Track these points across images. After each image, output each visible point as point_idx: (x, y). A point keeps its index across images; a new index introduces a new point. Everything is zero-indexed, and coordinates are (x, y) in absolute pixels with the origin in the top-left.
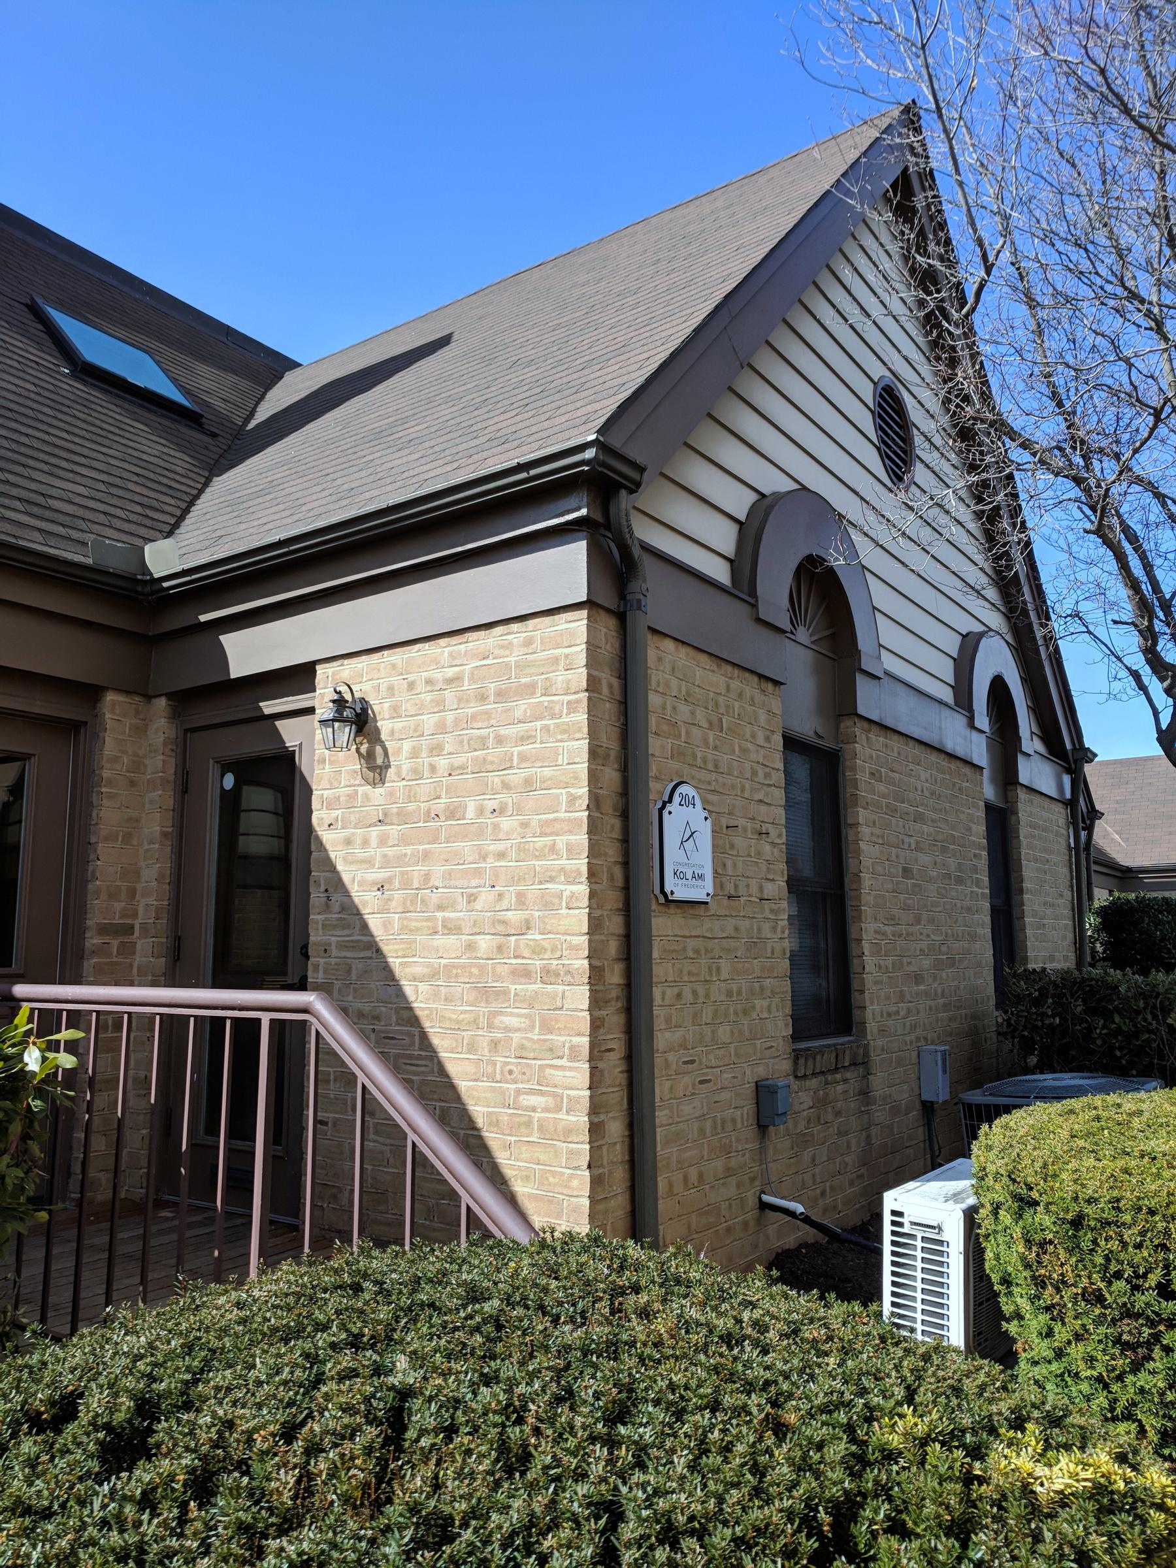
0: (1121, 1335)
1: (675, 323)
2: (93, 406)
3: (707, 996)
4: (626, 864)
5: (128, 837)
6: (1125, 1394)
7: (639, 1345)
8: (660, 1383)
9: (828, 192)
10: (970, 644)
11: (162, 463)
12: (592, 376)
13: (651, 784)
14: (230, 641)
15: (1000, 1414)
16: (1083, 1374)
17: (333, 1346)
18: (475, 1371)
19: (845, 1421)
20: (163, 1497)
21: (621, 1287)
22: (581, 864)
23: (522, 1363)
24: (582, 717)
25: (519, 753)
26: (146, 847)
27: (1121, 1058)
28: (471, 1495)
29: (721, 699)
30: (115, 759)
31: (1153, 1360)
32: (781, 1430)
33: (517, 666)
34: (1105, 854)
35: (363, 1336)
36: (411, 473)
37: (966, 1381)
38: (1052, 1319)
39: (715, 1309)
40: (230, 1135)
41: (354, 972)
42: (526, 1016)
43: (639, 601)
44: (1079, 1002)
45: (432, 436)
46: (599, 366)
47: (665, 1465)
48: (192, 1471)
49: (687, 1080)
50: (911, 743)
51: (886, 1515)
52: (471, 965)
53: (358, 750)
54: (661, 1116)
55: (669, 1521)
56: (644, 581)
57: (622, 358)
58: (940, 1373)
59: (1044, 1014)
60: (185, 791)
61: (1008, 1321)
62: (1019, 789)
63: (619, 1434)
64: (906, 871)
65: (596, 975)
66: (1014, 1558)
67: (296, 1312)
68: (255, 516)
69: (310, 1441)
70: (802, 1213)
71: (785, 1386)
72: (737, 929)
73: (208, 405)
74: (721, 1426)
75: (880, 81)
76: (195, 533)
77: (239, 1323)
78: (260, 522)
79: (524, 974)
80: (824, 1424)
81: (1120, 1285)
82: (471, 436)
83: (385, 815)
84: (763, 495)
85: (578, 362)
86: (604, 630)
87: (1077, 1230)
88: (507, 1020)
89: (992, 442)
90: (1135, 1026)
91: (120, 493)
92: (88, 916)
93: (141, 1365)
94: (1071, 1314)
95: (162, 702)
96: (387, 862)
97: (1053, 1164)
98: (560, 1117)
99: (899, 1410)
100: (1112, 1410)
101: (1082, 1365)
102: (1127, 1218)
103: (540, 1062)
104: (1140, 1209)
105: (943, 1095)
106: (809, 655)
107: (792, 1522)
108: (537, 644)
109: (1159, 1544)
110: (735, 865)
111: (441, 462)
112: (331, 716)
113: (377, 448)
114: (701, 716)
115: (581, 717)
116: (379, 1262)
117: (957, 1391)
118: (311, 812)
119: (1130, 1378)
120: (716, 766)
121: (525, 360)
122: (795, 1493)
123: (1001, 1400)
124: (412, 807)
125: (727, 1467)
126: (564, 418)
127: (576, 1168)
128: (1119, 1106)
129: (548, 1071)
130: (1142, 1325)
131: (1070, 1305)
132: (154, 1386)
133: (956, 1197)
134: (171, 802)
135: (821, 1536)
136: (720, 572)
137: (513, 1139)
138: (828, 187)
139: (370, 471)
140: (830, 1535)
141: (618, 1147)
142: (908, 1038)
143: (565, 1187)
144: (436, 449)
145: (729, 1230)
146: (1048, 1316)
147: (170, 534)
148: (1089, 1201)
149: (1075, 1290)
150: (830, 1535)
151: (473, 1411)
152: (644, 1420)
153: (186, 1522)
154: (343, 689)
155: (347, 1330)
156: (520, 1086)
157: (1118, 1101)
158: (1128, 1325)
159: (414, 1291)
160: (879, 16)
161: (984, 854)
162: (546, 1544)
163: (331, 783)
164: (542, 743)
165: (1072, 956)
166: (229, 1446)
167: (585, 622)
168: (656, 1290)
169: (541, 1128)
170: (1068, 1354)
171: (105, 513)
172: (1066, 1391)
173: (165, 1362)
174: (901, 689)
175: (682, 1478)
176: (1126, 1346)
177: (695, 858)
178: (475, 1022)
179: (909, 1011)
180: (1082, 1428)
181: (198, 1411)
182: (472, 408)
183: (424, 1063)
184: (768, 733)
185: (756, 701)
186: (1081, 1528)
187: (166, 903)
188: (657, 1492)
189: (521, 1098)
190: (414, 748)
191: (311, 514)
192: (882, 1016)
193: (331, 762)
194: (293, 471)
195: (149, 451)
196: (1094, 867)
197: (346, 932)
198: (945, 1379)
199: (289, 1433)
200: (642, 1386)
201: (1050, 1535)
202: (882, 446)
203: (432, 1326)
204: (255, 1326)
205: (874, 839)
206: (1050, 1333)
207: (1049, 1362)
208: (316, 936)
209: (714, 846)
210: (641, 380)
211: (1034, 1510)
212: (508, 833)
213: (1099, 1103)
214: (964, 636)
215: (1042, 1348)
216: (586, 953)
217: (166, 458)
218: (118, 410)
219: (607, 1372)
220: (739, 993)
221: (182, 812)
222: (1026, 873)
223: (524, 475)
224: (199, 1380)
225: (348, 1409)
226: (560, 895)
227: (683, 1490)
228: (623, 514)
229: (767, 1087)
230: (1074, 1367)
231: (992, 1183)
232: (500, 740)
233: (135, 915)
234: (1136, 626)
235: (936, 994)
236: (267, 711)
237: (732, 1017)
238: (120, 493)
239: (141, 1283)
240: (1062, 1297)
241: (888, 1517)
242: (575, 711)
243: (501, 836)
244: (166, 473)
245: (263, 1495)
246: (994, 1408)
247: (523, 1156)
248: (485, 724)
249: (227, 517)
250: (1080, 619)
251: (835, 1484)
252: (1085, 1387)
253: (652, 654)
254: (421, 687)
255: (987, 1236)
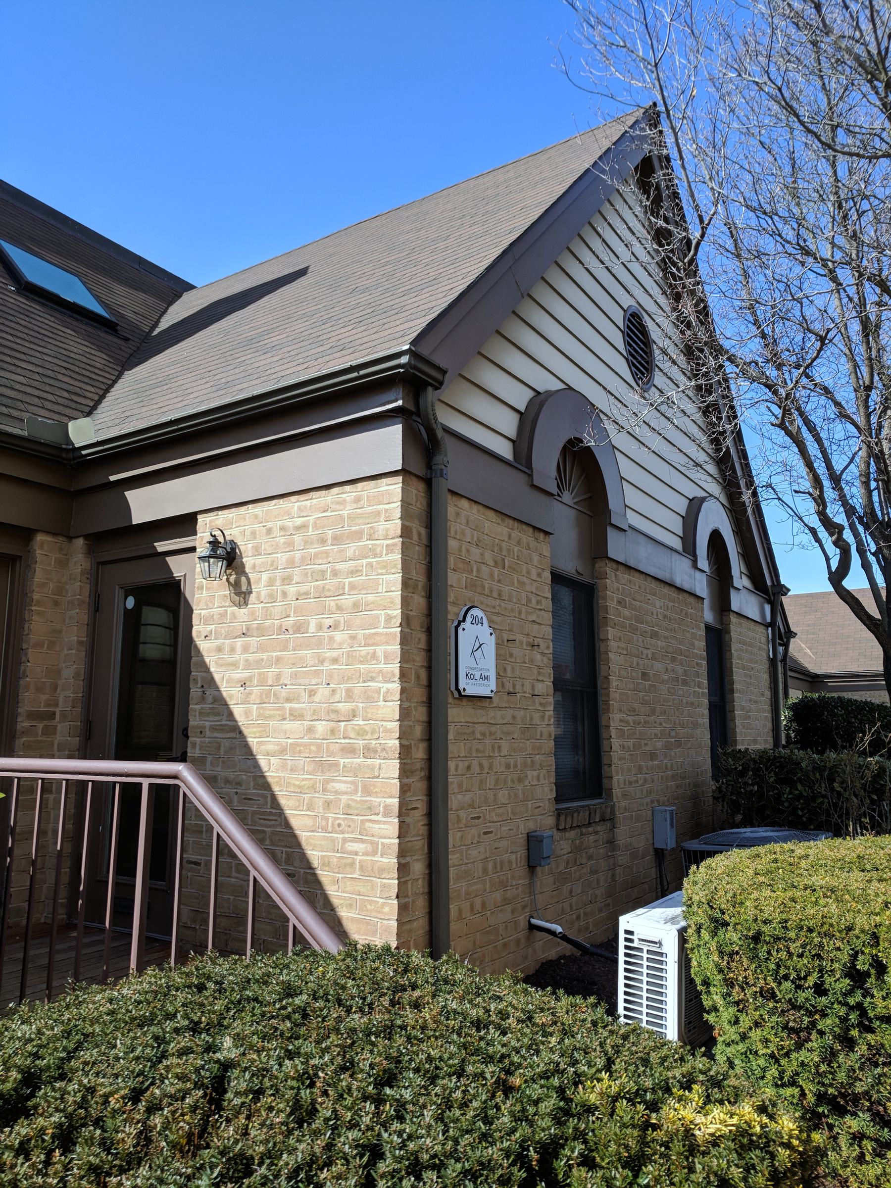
0: (788, 1022)
1: (472, 263)
2: (33, 316)
3: (490, 768)
4: (429, 668)
5: (52, 644)
6: (790, 1066)
7: (409, 1028)
8: (420, 1056)
9: (588, 170)
10: (695, 505)
11: (85, 360)
12: (410, 301)
13: (449, 607)
14: (132, 496)
15: (674, 1078)
16: (761, 1052)
17: (177, 1031)
18: (282, 1048)
19: (557, 1085)
20: (35, 1147)
21: (402, 986)
22: (395, 667)
23: (318, 1042)
24: (397, 557)
25: (350, 583)
26: (66, 652)
27: (802, 816)
28: (268, 1141)
29: (504, 545)
30: (43, 585)
31: (811, 1041)
32: (508, 1090)
33: (349, 518)
34: (799, 664)
35: (201, 1023)
36: (273, 371)
37: (653, 1054)
38: (738, 1011)
39: (470, 1002)
40: (117, 872)
41: (222, 748)
42: (352, 783)
43: (442, 470)
44: (772, 774)
45: (290, 343)
46: (415, 294)
47: (418, 1117)
48: (59, 1126)
49: (474, 831)
50: (649, 579)
51: (580, 1154)
52: (311, 744)
53: (228, 580)
54: (453, 859)
55: (417, 1158)
56: (446, 455)
57: (432, 288)
58: (634, 1048)
59: (746, 783)
60: (97, 610)
61: (708, 1013)
62: (731, 614)
63: (385, 1094)
64: (645, 676)
65: (405, 752)
66: (672, 1184)
67: (152, 1005)
68: (154, 401)
69: (151, 1102)
70: (560, 933)
71: (516, 1059)
72: (514, 717)
73: (122, 316)
74: (464, 1088)
75: (624, 89)
76: (109, 413)
77: (108, 1014)
78: (158, 406)
79: (350, 751)
80: (542, 1087)
81: (787, 985)
82: (318, 344)
83: (248, 629)
84: (538, 393)
85: (400, 290)
86: (415, 492)
87: (756, 943)
88: (337, 786)
89: (705, 357)
90: (812, 792)
91: (52, 382)
92: (20, 705)
93: (29, 1047)
94: (752, 1007)
95: (80, 542)
96: (248, 665)
97: (740, 895)
98: (376, 859)
99: (599, 1075)
100: (781, 1078)
101: (760, 1046)
102: (792, 935)
103: (362, 818)
104: (802, 928)
105: (671, 844)
106: (572, 513)
107: (508, 1157)
108: (364, 501)
109: (785, 1174)
110: (513, 669)
111: (295, 363)
112: (207, 554)
113: (248, 352)
114: (488, 557)
115: (396, 557)
116: (221, 967)
117: (646, 1062)
118: (192, 626)
119: (794, 1055)
120: (500, 595)
121: (362, 288)
122: (513, 1138)
123: (676, 1067)
124: (268, 623)
125: (463, 1118)
126: (387, 332)
127: (387, 898)
128: (793, 851)
129: (367, 824)
130: (803, 1015)
131: (751, 1000)
132: (38, 1062)
133: (673, 920)
134: (86, 617)
135: (530, 1169)
136: (504, 450)
137: (341, 876)
138: (588, 166)
139: (242, 369)
140: (537, 1168)
141: (420, 882)
142: (645, 801)
143: (379, 912)
144: (292, 353)
145: (505, 945)
146: (736, 1009)
147: (89, 414)
148: (766, 922)
149: (755, 989)
150: (537, 1168)
151: (277, 1078)
152: (407, 1084)
153: (50, 1164)
154: (217, 533)
155: (188, 1019)
156: (347, 836)
157: (792, 848)
158: (793, 1015)
159: (245, 989)
160: (624, 41)
161: (704, 663)
162: (322, 1176)
163: (207, 605)
164: (367, 575)
165: (770, 740)
166: (90, 1107)
167: (401, 485)
168: (430, 988)
169: (362, 868)
170: (750, 1037)
171: (39, 397)
172: (748, 1065)
173: (48, 1044)
174: (642, 539)
175: (429, 1127)
176: (791, 1030)
177: (482, 664)
178: (313, 787)
179: (645, 780)
180: (735, 1088)
181: (70, 1080)
182: (320, 323)
183: (274, 818)
184: (540, 570)
185: (531, 545)
186: (725, 1162)
187: (81, 695)
188: (410, 1137)
189: (347, 845)
190: (270, 578)
191: (196, 401)
192: (625, 784)
193: (207, 589)
194: (185, 368)
195: (75, 350)
196: (789, 673)
197: (217, 718)
198: (637, 1053)
199: (136, 1096)
200: (407, 1058)
201: (701, 1167)
202: (630, 358)
203: (254, 1015)
204: (120, 1016)
205: (620, 651)
206: (737, 1022)
207: (737, 1043)
208: (194, 722)
209: (497, 655)
210: (445, 305)
211: (692, 1149)
212: (340, 644)
213: (778, 849)
214: (690, 500)
215: (731, 1033)
216: (397, 735)
217: (88, 356)
218: (52, 319)
219: (380, 1048)
220: (515, 766)
221: (94, 625)
222: (736, 678)
223: (355, 375)
224: (73, 1057)
225: (182, 1078)
226: (378, 691)
227: (429, 1135)
228: (429, 404)
229: (536, 837)
230: (754, 1047)
231: (696, 909)
232: (335, 573)
233: (57, 705)
234: (811, 495)
235: (666, 768)
236: (160, 550)
237: (509, 784)
238: (52, 382)
239: (47, 989)
240: (745, 994)
241: (581, 1155)
242: (392, 552)
243: (335, 646)
244: (88, 367)
245: (112, 1144)
246: (670, 1074)
247: (347, 889)
248: (325, 561)
249: (134, 401)
250: (773, 488)
251: (543, 1130)
252: (762, 1062)
253: (451, 510)
254: (276, 532)
255: (692, 949)
